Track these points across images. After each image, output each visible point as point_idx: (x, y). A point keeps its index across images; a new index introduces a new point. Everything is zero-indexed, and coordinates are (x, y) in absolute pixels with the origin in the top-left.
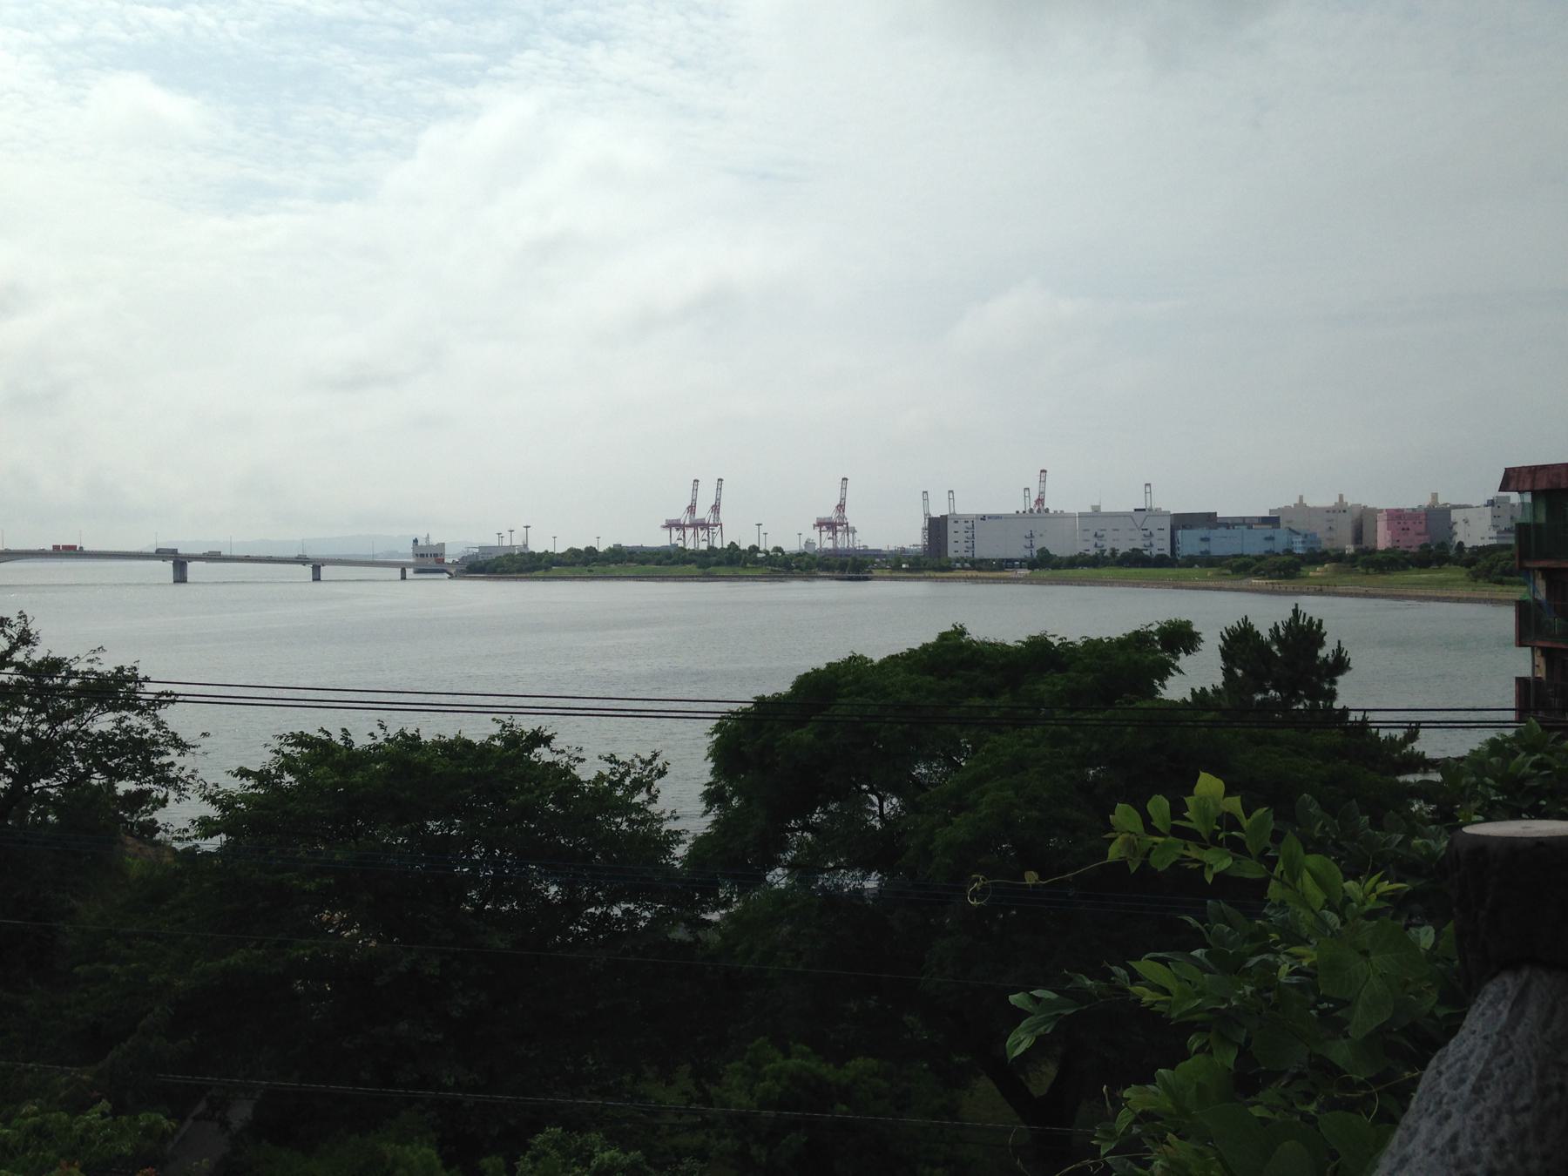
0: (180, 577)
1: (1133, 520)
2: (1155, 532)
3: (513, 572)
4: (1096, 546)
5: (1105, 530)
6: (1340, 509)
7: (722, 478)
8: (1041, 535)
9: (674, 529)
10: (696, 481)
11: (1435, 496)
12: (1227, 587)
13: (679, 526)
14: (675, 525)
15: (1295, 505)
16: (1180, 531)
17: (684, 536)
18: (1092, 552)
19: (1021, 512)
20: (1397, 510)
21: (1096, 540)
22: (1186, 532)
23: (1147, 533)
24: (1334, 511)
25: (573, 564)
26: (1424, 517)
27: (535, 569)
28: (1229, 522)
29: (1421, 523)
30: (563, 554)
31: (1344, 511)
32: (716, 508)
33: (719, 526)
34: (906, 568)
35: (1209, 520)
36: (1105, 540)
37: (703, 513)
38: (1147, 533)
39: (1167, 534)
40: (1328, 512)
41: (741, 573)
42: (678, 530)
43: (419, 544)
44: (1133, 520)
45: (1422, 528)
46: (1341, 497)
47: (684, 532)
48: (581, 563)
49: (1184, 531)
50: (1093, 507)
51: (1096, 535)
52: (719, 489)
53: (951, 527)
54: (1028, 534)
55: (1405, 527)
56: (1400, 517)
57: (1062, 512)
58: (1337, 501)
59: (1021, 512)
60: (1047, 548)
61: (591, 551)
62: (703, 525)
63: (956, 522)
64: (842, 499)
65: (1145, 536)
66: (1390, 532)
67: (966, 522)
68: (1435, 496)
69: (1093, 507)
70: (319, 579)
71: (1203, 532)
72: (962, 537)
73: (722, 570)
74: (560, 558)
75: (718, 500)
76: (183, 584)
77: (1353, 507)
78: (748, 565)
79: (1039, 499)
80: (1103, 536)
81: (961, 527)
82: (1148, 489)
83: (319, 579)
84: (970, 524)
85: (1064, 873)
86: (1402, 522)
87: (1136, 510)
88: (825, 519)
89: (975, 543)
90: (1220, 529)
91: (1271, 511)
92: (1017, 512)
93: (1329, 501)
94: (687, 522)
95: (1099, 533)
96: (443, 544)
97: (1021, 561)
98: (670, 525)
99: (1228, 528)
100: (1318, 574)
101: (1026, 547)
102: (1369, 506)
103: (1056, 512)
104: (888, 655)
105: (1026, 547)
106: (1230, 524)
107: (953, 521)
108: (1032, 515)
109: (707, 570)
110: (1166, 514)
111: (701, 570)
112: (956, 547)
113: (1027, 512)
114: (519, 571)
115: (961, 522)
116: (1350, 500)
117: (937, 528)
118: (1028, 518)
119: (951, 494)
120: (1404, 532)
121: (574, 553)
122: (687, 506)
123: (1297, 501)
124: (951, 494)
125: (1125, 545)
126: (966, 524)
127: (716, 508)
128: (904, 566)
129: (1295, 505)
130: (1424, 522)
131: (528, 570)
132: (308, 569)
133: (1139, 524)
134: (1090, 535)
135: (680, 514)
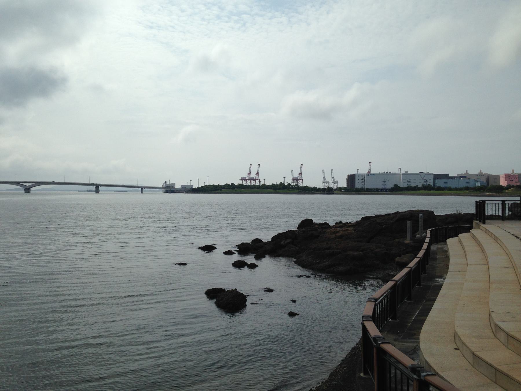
0: (97, 191)
1: (421, 176)
2: (428, 180)
3: (209, 191)
4: (408, 184)
5: (411, 179)
6: (481, 175)
7: (252, 164)
8: (388, 181)
9: (243, 181)
10: (259, 164)
11: (513, 171)
12: (479, 195)
13: (245, 180)
14: (244, 179)
15: (465, 173)
16: (437, 180)
17: (247, 183)
18: (407, 186)
19: (381, 173)
20: (508, 174)
21: (408, 183)
22: (440, 180)
23: (426, 180)
24: (479, 175)
25: (229, 189)
26: (517, 176)
27: (218, 190)
28: (453, 177)
29: (516, 178)
30: (224, 186)
31: (483, 175)
32: (257, 174)
33: (259, 180)
34: (344, 191)
35: (446, 176)
36: (411, 183)
37: (253, 175)
38: (426, 180)
39: (432, 180)
40: (478, 175)
41: (288, 192)
42: (253, 181)
43: (167, 183)
44: (421, 176)
45: (517, 180)
46: (481, 171)
47: (247, 182)
48: (231, 188)
49: (438, 180)
50: (405, 172)
51: (408, 181)
52: (259, 167)
53: (357, 178)
54: (384, 181)
55: (512, 180)
56: (510, 176)
57: (395, 173)
58: (479, 172)
59: (381, 173)
60: (397, 184)
61: (233, 184)
62: (254, 180)
63: (359, 176)
64: (301, 171)
65: (425, 181)
66: (506, 181)
67: (362, 176)
68: (513, 171)
69: (405, 172)
70: (142, 193)
71: (445, 180)
72: (360, 181)
73: (281, 191)
74: (223, 187)
75: (258, 171)
76: (176, 184)
77: (485, 174)
78: (290, 189)
79: (369, 172)
80: (410, 181)
81: (360, 178)
82: (400, 170)
83: (142, 193)
84: (363, 177)
85: (27, 376)
86: (510, 178)
87: (420, 173)
88: (295, 177)
89: (365, 184)
90: (450, 179)
91: (457, 175)
92: (380, 173)
93: (477, 172)
94: (248, 178)
95: (409, 180)
96: (175, 183)
97: (382, 189)
98: (242, 179)
99: (453, 179)
100: (509, 191)
101: (383, 185)
102: (490, 174)
103: (393, 173)
104: (338, 219)
105: (383, 185)
106: (453, 178)
107: (361, 176)
108: (384, 174)
109: (276, 191)
110: (432, 174)
111: (274, 191)
112: (358, 185)
113: (383, 173)
114: (211, 191)
115: (360, 176)
116: (484, 172)
117: (351, 178)
118: (381, 175)
119: (332, 171)
120: (511, 181)
121: (227, 185)
122: (256, 173)
123: (465, 172)
124: (332, 171)
125: (419, 183)
126: (362, 177)
127: (257, 174)
128: (343, 190)
129: (465, 173)
130: (518, 178)
131: (214, 190)
132: (140, 189)
133: (423, 177)
134: (406, 181)
135: (245, 176)
